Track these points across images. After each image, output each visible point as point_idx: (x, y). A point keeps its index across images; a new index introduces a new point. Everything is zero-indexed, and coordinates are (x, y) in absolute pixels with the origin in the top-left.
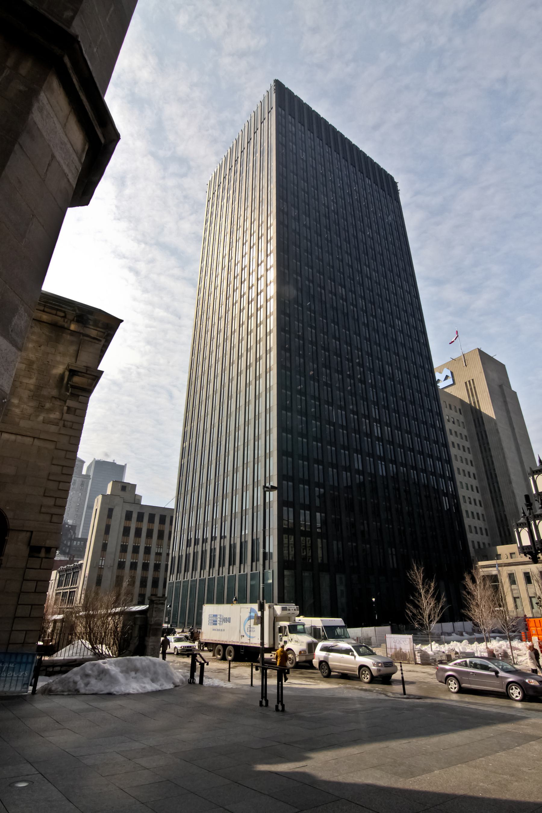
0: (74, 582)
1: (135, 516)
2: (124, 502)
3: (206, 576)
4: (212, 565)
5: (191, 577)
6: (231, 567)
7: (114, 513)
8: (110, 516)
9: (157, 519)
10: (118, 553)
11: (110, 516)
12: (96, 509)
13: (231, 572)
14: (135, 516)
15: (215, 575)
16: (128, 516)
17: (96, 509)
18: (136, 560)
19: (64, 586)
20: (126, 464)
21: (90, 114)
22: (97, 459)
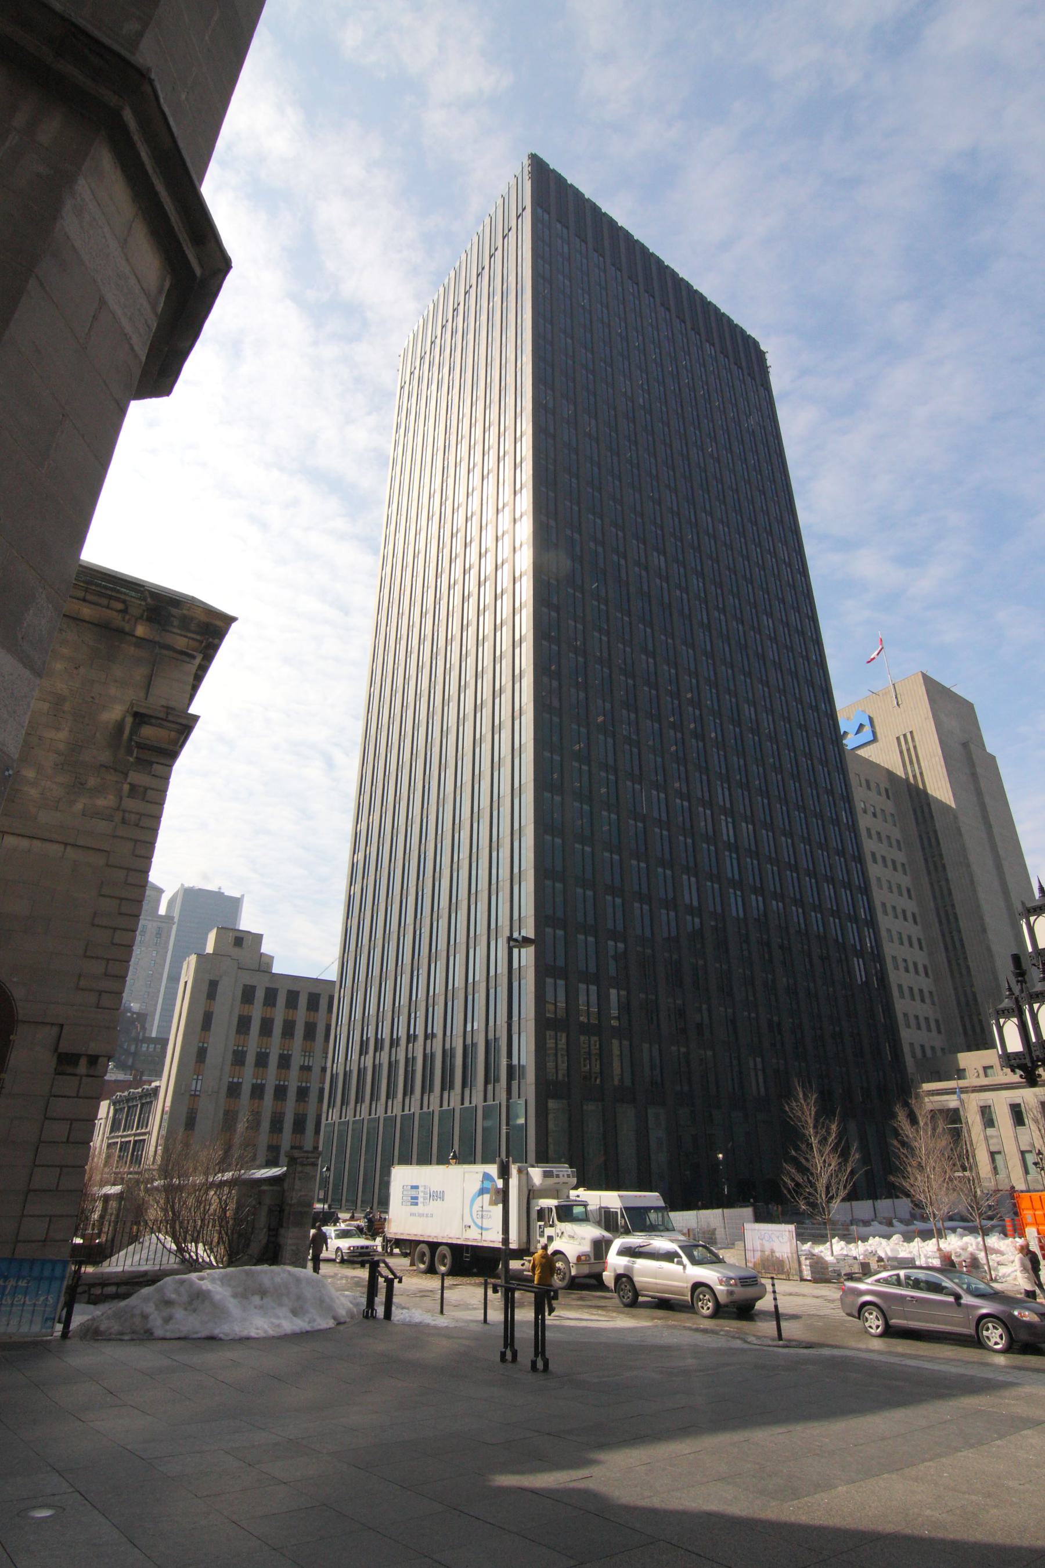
0: (143, 1122)
1: (260, 994)
2: (239, 968)
3: (397, 1111)
7: (220, 989)
8: (212, 994)
10: (228, 1068)
11: (212, 994)
12: (186, 982)
14: (260, 994)
17: (186, 982)
18: (262, 1079)
19: (124, 1130)
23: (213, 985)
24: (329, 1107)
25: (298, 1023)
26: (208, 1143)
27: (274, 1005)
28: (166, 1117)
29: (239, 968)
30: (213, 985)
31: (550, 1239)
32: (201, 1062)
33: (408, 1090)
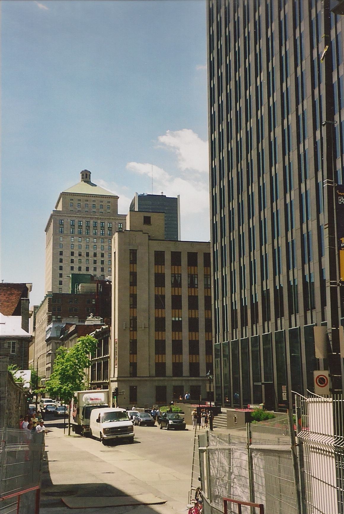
0: (106, 351)
1: (168, 257)
2: (149, 240)
3: (260, 333)
4: (267, 318)
5: (321, 319)
6: (309, 313)
7: (138, 255)
8: (133, 261)
9: (200, 260)
10: (153, 311)
11: (133, 261)
12: (115, 253)
13: (266, 330)
14: (168, 257)
15: (272, 330)
16: (159, 257)
17: (115, 253)
18: (179, 318)
19: (97, 357)
20: (179, 196)
21: (284, 39)
22: (139, 194)
23: (133, 253)
24: (214, 271)
25: (203, 308)
26: (336, 453)
27: (189, 297)
28: (117, 345)
29: (149, 240)
30: (133, 253)
31: (59, 407)
32: (133, 308)
33: (267, 318)
